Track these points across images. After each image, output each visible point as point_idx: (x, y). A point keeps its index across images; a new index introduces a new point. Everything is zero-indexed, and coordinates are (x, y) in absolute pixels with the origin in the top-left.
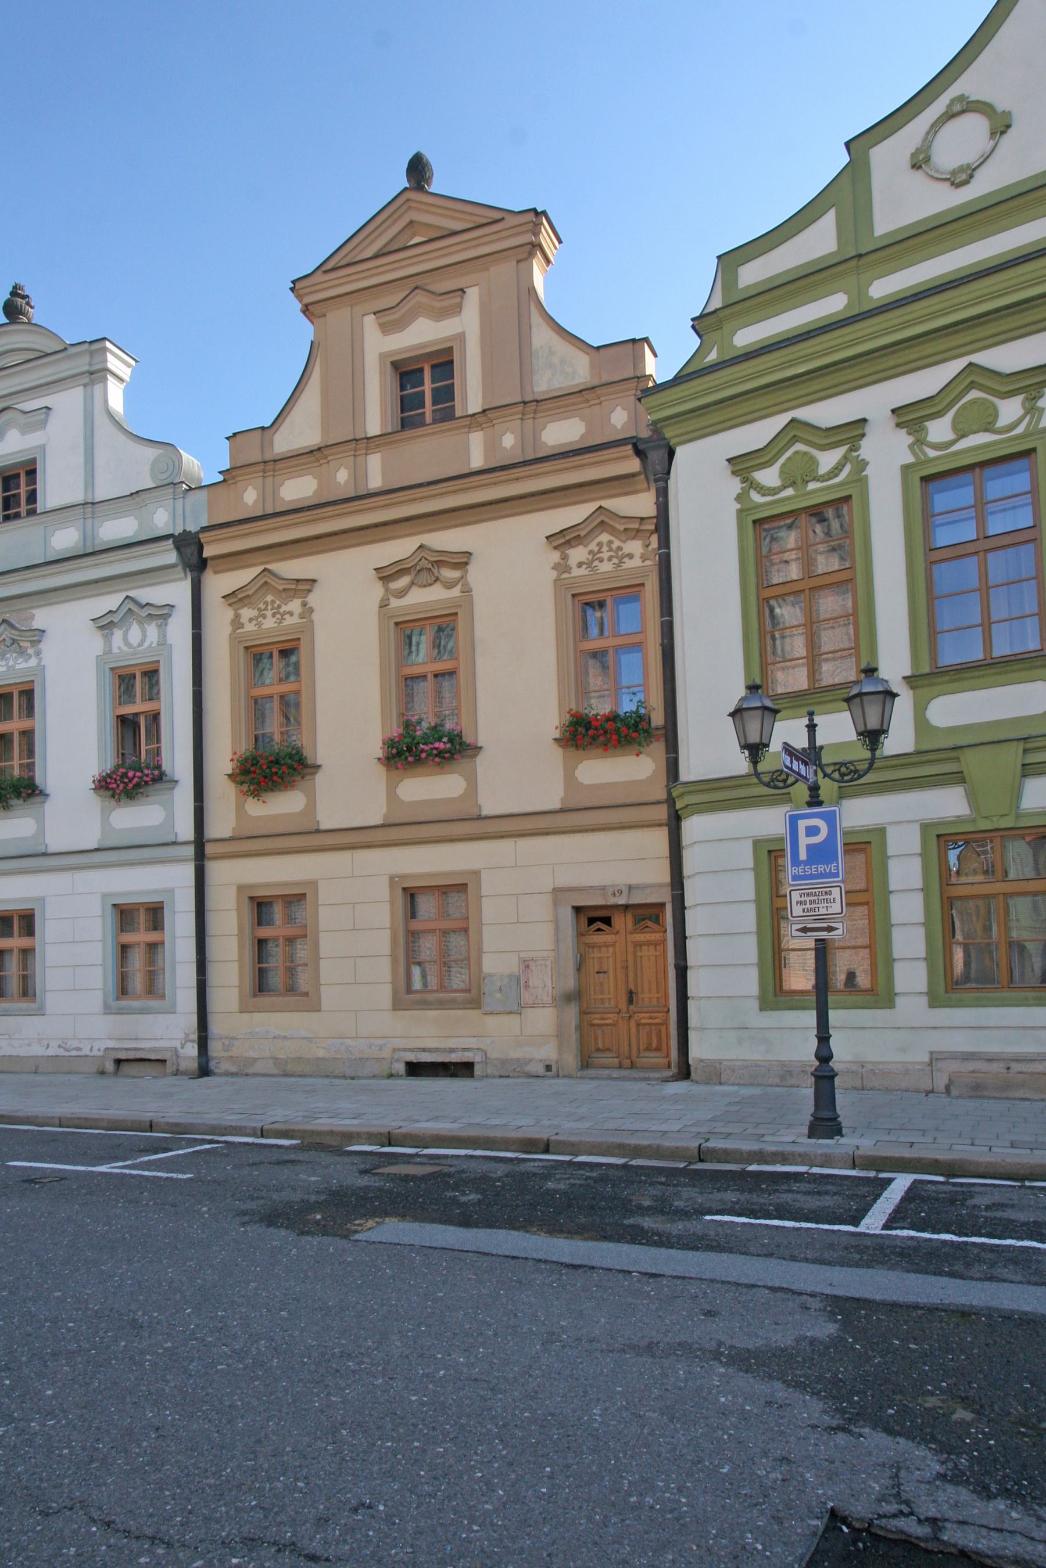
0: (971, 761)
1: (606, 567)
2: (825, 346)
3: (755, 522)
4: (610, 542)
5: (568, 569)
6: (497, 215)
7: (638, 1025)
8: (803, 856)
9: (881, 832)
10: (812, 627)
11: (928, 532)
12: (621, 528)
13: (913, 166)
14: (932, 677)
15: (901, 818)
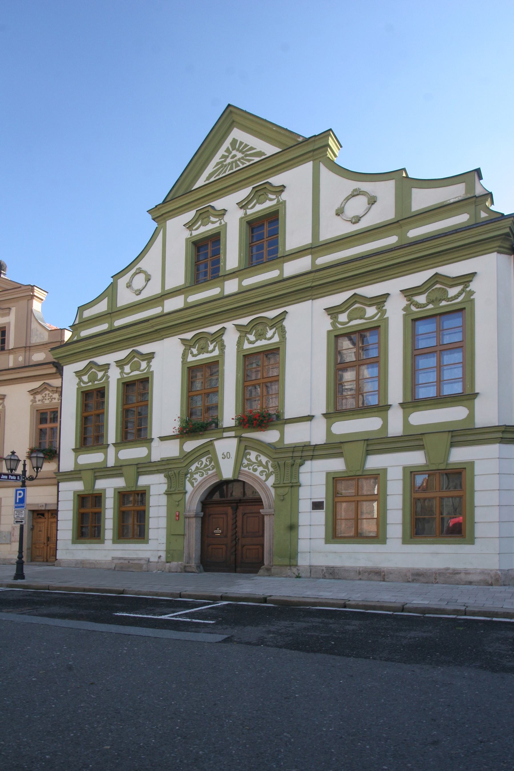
0: (346, 448)
1: (47, 402)
2: (367, 263)
3: (412, 320)
4: (49, 394)
5: (35, 402)
6: (19, 286)
7: (50, 548)
8: (18, 501)
9: (385, 470)
10: (440, 368)
11: (413, 344)
12: (51, 390)
13: (337, 214)
14: (412, 403)
15: (394, 465)
